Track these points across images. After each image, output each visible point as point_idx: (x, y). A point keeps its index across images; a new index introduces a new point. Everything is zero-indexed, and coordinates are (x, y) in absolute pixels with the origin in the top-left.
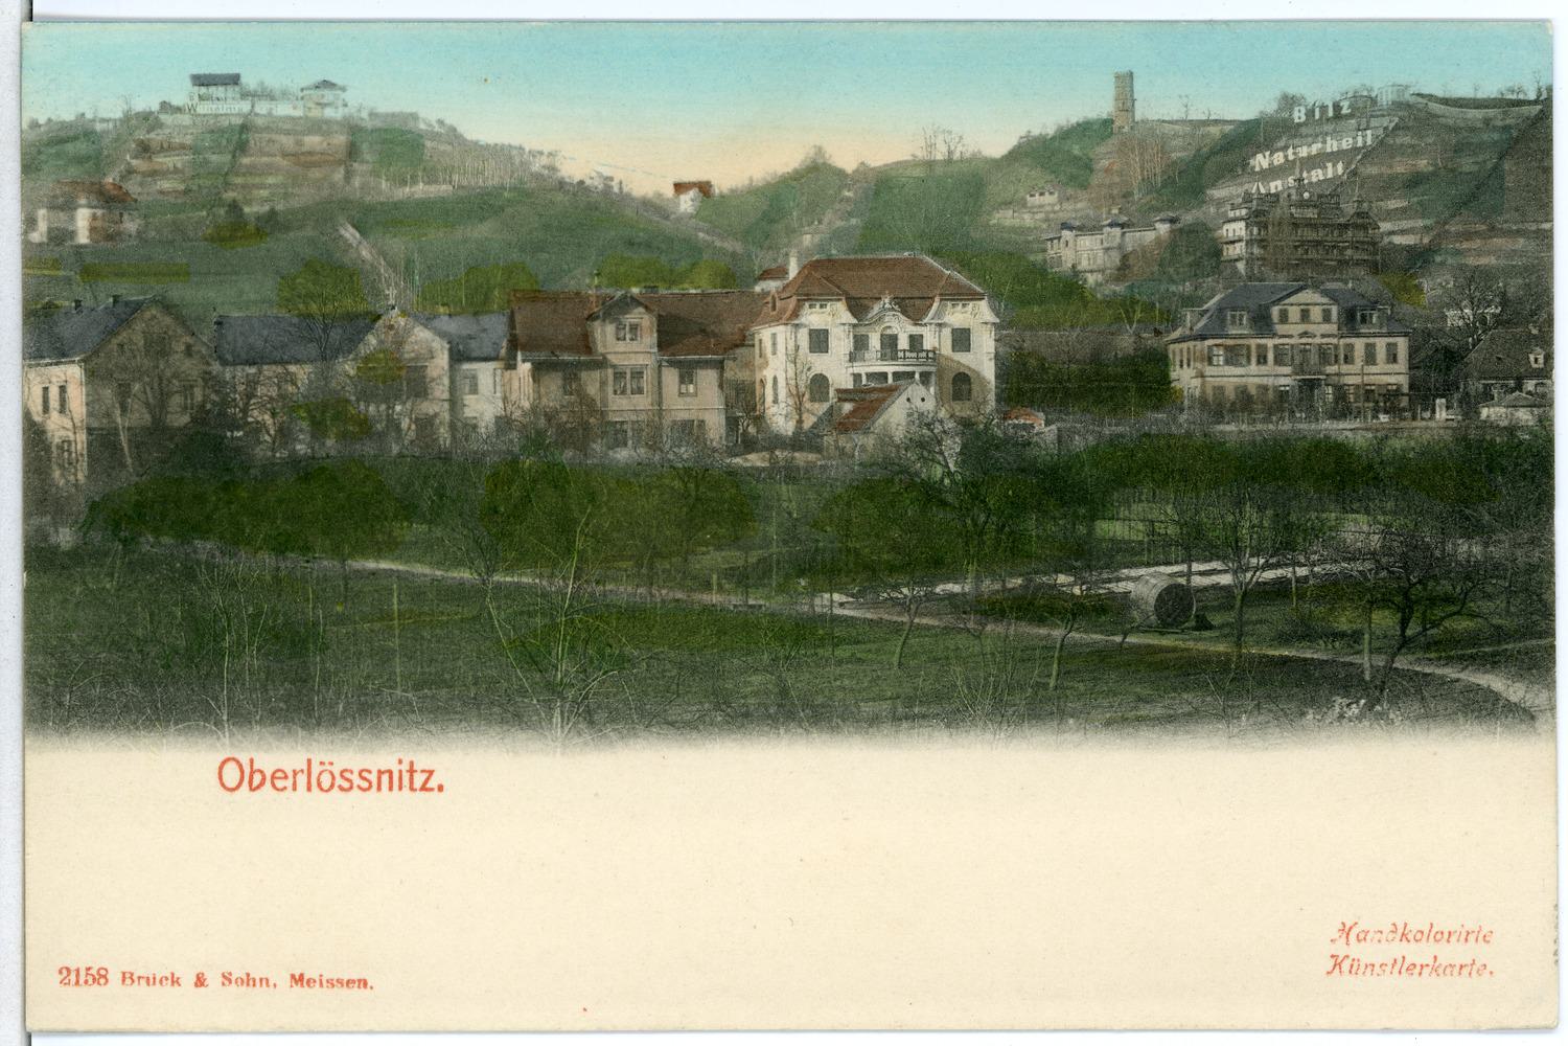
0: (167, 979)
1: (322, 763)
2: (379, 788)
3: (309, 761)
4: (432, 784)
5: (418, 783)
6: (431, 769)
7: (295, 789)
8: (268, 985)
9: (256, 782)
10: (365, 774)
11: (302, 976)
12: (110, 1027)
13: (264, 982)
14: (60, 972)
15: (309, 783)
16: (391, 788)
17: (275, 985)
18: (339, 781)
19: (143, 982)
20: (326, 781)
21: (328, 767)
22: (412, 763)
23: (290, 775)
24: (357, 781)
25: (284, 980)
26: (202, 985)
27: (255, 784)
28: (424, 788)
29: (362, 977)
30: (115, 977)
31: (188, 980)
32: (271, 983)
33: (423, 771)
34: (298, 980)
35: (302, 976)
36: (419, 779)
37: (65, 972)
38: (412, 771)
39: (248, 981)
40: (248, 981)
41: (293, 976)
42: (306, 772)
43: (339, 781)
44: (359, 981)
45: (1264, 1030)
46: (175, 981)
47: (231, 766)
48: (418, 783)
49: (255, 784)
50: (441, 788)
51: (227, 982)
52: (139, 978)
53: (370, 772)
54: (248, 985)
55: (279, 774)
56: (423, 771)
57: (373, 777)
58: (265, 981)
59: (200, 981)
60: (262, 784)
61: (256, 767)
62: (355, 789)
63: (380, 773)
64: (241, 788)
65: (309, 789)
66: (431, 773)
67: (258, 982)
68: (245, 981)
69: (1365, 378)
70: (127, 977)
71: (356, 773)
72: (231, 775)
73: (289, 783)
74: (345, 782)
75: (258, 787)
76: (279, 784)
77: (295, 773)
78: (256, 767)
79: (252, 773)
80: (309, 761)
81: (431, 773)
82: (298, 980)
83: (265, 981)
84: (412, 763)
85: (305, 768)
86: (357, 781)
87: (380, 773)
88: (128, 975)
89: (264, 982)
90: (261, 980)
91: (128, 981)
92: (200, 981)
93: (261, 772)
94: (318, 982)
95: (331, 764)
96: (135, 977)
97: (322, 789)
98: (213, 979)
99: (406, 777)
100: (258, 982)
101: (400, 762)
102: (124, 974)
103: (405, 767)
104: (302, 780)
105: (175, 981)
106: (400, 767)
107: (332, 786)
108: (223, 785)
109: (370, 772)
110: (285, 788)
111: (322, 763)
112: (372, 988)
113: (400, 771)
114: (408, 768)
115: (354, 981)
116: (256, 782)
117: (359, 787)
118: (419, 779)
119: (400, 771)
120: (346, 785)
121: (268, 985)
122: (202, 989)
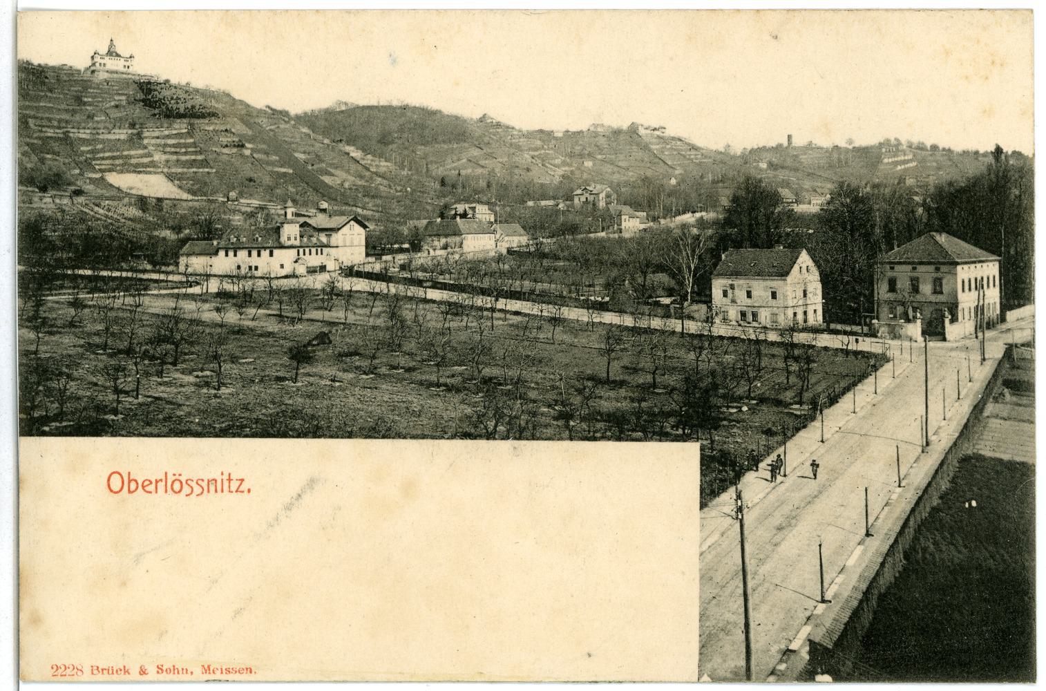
4: (244, 487)
10: (200, 482)
14: (52, 668)
17: (192, 673)
20: (177, 486)
21: (177, 477)
26: (144, 673)
31: (135, 671)
36: (234, 485)
37: (55, 667)
38: (230, 480)
42: (164, 483)
48: (233, 488)
50: (249, 491)
51: (160, 671)
52: (103, 670)
57: (205, 484)
59: (143, 672)
60: (137, 488)
63: (209, 481)
65: (166, 491)
66: (242, 480)
71: (195, 481)
72: (116, 483)
75: (133, 492)
79: (130, 481)
81: (242, 480)
85: (164, 478)
89: (176, 671)
91: (95, 672)
92: (143, 672)
93: (136, 481)
95: (180, 475)
96: (100, 669)
98: (152, 670)
99: (226, 484)
100: (181, 672)
101: (222, 474)
103: (226, 477)
108: (111, 491)
109: (203, 480)
111: (174, 475)
118: (234, 485)
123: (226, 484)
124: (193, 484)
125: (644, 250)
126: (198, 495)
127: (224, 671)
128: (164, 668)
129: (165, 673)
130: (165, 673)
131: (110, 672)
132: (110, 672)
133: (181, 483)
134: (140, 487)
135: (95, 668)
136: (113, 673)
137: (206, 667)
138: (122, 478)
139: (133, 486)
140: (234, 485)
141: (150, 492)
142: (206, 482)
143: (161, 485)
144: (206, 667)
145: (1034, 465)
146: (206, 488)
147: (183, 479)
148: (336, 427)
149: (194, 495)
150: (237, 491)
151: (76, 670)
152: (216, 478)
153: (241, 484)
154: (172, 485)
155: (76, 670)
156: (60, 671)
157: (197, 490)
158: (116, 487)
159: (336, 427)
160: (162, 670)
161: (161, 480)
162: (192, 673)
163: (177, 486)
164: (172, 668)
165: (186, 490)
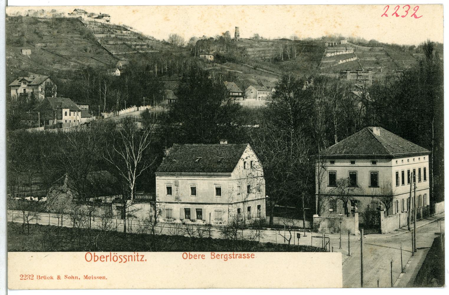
2: (129, 261)
7: (199, 258)
9: (96, 259)
10: (125, 257)
11: (87, 276)
13: (76, 278)
16: (132, 260)
17: (79, 279)
19: (43, 278)
20: (115, 259)
21: (115, 255)
25: (82, 278)
28: (141, 261)
30: (35, 277)
31: (55, 277)
32: (78, 278)
33: (141, 256)
34: (86, 277)
35: (87, 276)
36: (140, 258)
37: (22, 276)
39: (72, 277)
40: (72, 277)
41: (53, 279)
45: (327, 288)
46: (52, 278)
50: (146, 260)
51: (66, 278)
53: (126, 256)
56: (141, 256)
57: (127, 258)
58: (76, 278)
59: (59, 278)
60: (98, 259)
63: (129, 256)
64: (92, 261)
67: (75, 278)
68: (30, 84)
69: (318, 167)
70: (39, 277)
73: (197, 257)
75: (96, 261)
77: (107, 257)
79: (95, 256)
82: (86, 277)
83: (76, 278)
89: (76, 278)
90: (76, 277)
91: (39, 278)
92: (59, 278)
94: (91, 278)
97: (114, 261)
98: (62, 277)
99: (136, 257)
100: (75, 278)
102: (37, 276)
105: (52, 278)
106: (134, 254)
108: (87, 261)
109: (126, 256)
110: (104, 261)
113: (135, 256)
114: (137, 255)
115: (101, 277)
116: (96, 259)
117: (247, 258)
118: (140, 258)
119: (135, 256)
120: (244, 257)
123: (136, 257)
124: (122, 257)
126: (124, 262)
127: (93, 278)
128: (68, 277)
131: (45, 278)
132: (45, 278)
134: (193, 257)
135: (38, 276)
137: (86, 276)
138: (92, 256)
141: (196, 258)
142: (128, 257)
143: (109, 258)
146: (128, 260)
149: (123, 262)
150: (141, 261)
153: (142, 259)
154: (113, 258)
156: (24, 277)
157: (124, 260)
158: (89, 259)
161: (108, 256)
162: (79, 279)
165: (119, 260)
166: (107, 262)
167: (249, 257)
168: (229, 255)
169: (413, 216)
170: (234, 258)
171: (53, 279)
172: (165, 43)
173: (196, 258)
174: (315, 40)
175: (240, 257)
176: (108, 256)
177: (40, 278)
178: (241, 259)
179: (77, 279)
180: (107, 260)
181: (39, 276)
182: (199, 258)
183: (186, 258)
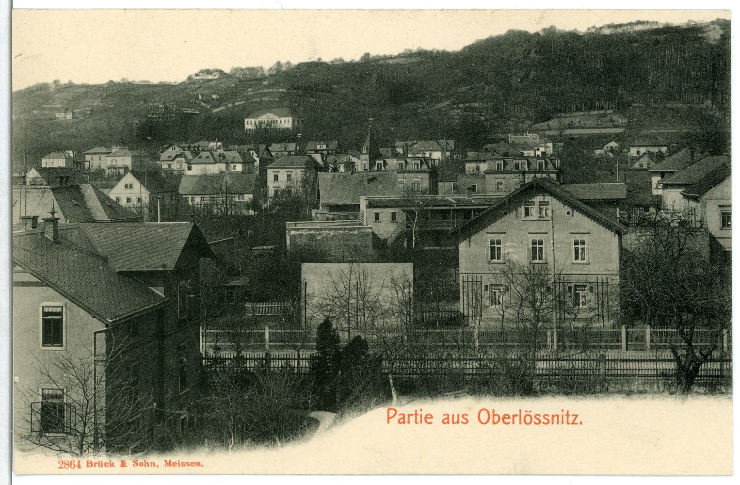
0: (108, 463)
1: (526, 411)
3: (520, 411)
4: (577, 421)
5: (571, 421)
6: (577, 414)
7: (513, 423)
8: (154, 466)
10: (546, 417)
12: (7, 31)
14: (59, 462)
15: (558, 421)
16: (558, 423)
18: (534, 420)
19: (97, 465)
20: (528, 419)
21: (528, 413)
22: (568, 412)
23: (511, 417)
24: (543, 420)
27: (495, 421)
28: (573, 423)
29: (197, 461)
32: (156, 465)
33: (573, 415)
35: (170, 461)
36: (571, 419)
37: (61, 463)
38: (568, 415)
43: (534, 420)
44: (197, 463)
47: (484, 412)
48: (571, 421)
49: (495, 421)
50: (581, 423)
51: (135, 465)
53: (548, 415)
54: (145, 466)
55: (429, 416)
56: (573, 415)
57: (550, 418)
60: (499, 420)
61: (495, 413)
62: (533, 423)
63: (553, 416)
65: (520, 423)
66: (577, 416)
71: (542, 415)
72: (484, 416)
73: (511, 420)
74: (537, 420)
75: (498, 422)
76: (506, 421)
77: (514, 416)
78: (495, 413)
79: (494, 415)
80: (520, 411)
81: (577, 416)
84: (568, 412)
85: (518, 413)
86: (543, 420)
87: (553, 416)
88: (90, 462)
90: (151, 463)
91: (90, 465)
93: (396, 411)
94: (177, 465)
95: (530, 412)
99: (565, 418)
100: (150, 465)
101: (563, 411)
103: (565, 413)
104: (517, 419)
106: (562, 413)
107: (531, 422)
109: (548, 415)
111: (421, 410)
112: (202, 466)
113: (563, 416)
115: (194, 463)
118: (571, 419)
119: (563, 416)
120: (537, 421)
121: (154, 466)
122: (124, 468)
125: (694, 69)
127: (181, 465)
129: (139, 466)
130: (139, 466)
133: (531, 417)
134: (501, 421)
135: (90, 462)
136: (102, 466)
137: (168, 461)
139: (496, 419)
140: (573, 420)
141: (508, 423)
143: (517, 419)
144: (168, 461)
145: (730, 252)
146: (551, 421)
147: (533, 414)
148: (218, 266)
150: (573, 423)
151: (64, 465)
152: (559, 414)
155: (64, 465)
159: (218, 266)
160: (137, 464)
161: (517, 415)
163: (528, 419)
164: (144, 463)
166: (563, 426)
167: (535, 417)
168: (463, 416)
169: (216, 335)
170: (568, 423)
171: (114, 466)
172: (119, 84)
173: (508, 423)
174: (438, 52)
175: (402, 421)
176: (517, 415)
177: (92, 465)
178: (403, 424)
179: (153, 467)
180: (515, 421)
181: (91, 462)
182: (513, 423)
183: (487, 422)
